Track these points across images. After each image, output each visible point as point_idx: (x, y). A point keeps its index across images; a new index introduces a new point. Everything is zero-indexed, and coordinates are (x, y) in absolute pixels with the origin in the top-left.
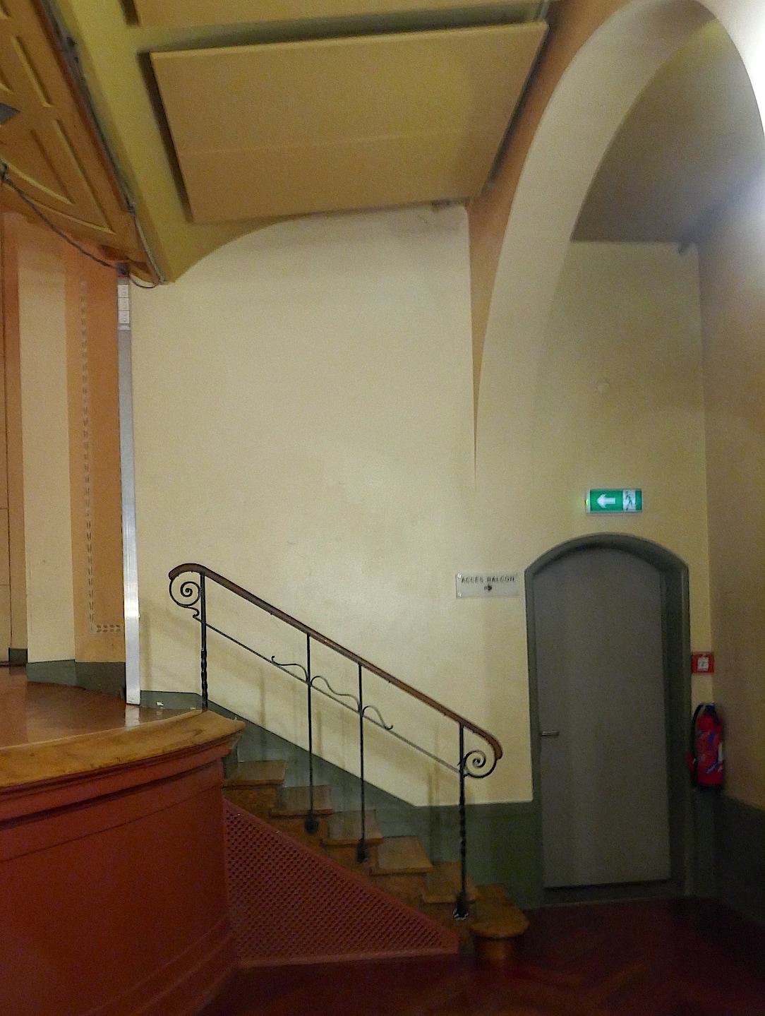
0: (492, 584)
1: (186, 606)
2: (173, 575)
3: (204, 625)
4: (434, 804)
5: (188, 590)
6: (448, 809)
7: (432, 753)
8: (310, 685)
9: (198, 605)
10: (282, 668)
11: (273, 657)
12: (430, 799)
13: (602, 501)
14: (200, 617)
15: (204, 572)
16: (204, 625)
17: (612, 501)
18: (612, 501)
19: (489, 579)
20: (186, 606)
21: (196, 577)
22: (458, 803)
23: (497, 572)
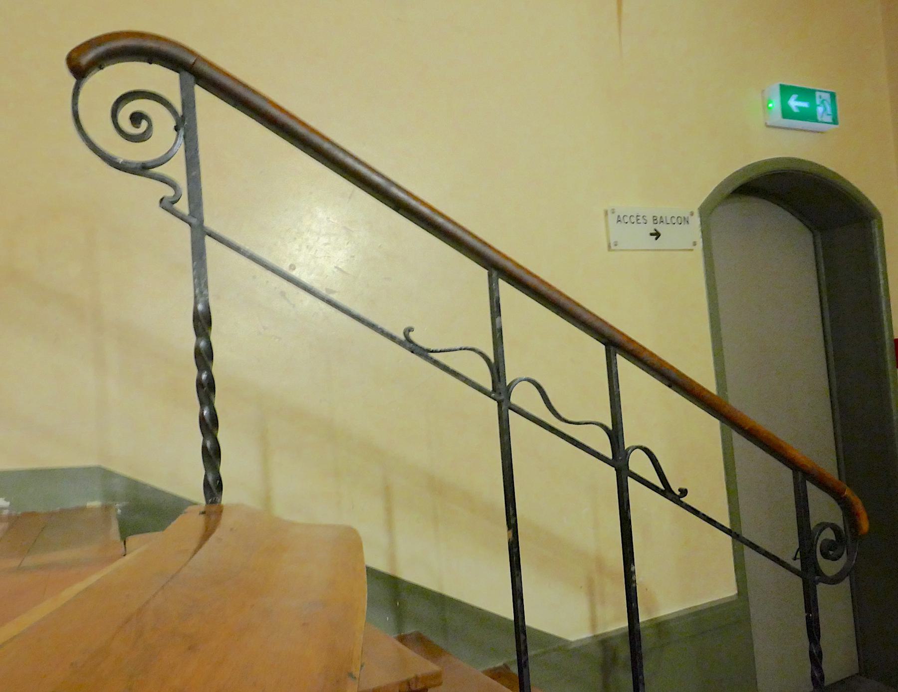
0: (660, 228)
1: (143, 169)
2: (80, 68)
3: (200, 234)
4: (600, 631)
5: (136, 118)
6: (617, 635)
7: (746, 548)
8: (505, 407)
9: (176, 170)
10: (436, 363)
11: (410, 330)
12: (594, 626)
13: (794, 103)
14: (183, 206)
15: (195, 72)
16: (200, 234)
17: (805, 105)
18: (805, 105)
19: (655, 219)
20: (143, 169)
21: (164, 80)
22: (625, 624)
23: (667, 209)
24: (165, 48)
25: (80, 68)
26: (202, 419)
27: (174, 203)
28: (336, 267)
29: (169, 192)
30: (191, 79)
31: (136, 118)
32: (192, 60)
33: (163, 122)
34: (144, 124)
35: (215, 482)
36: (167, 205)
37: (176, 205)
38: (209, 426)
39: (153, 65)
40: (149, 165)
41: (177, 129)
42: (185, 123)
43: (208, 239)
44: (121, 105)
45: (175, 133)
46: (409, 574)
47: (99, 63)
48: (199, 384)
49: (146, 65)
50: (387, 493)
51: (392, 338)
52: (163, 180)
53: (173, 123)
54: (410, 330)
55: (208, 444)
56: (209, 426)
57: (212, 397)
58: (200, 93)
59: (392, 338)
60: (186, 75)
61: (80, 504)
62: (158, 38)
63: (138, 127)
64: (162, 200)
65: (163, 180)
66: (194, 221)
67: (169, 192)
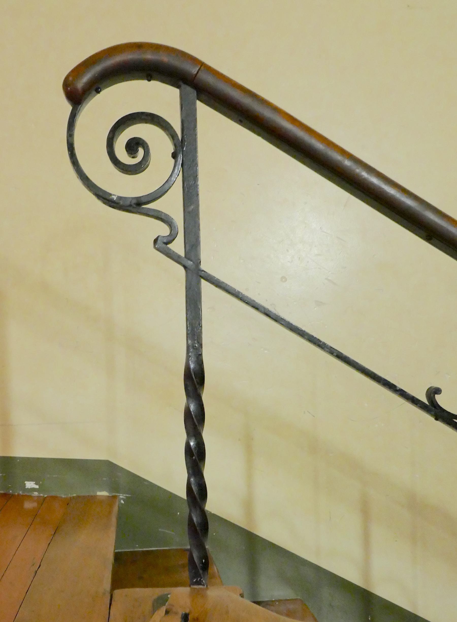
1: (136, 206)
2: (76, 96)
3: (196, 276)
5: (133, 145)
9: (172, 204)
11: (438, 391)
14: (178, 246)
16: (196, 276)
20: (136, 206)
21: (162, 98)
22: (196, 72)
24: (165, 58)
25: (76, 96)
26: (187, 413)
27: (167, 243)
28: (326, 279)
29: (163, 230)
30: (192, 92)
31: (133, 145)
32: (194, 70)
33: (160, 144)
34: (141, 152)
35: (200, 559)
36: (162, 245)
37: (169, 246)
38: (195, 421)
39: (153, 82)
40: (144, 200)
41: (174, 156)
42: (185, 148)
43: (204, 284)
44: (117, 133)
45: (173, 161)
46: (384, 590)
47: (96, 86)
48: (188, 450)
49: (144, 83)
50: (365, 511)
51: (414, 401)
52: (159, 216)
53: (171, 149)
54: (438, 391)
55: (192, 407)
56: (195, 421)
57: (200, 464)
58: (203, 111)
59: (414, 401)
60: (189, 89)
61: (84, 492)
62: (157, 48)
63: (133, 157)
64: (156, 241)
65: (159, 216)
66: (189, 263)
67: (163, 230)
